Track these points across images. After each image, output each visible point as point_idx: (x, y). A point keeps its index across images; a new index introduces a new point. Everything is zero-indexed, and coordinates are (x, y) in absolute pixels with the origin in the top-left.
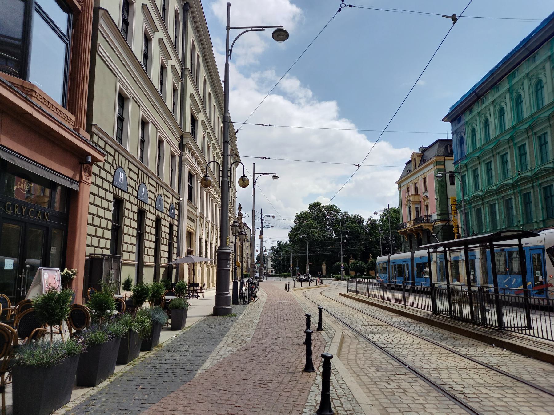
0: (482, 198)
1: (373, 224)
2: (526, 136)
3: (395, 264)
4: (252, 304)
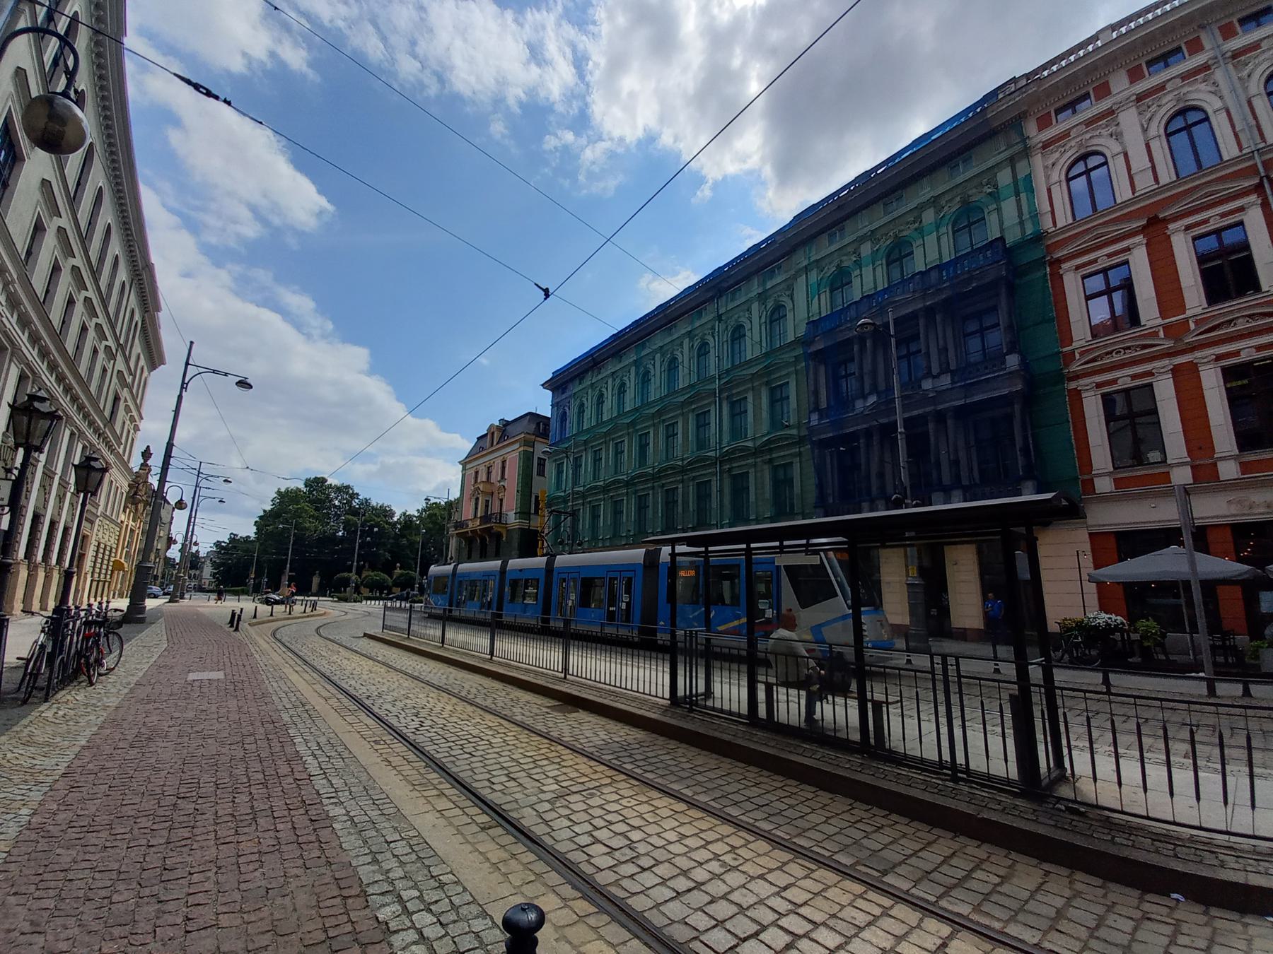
0: (583, 495)
1: (407, 521)
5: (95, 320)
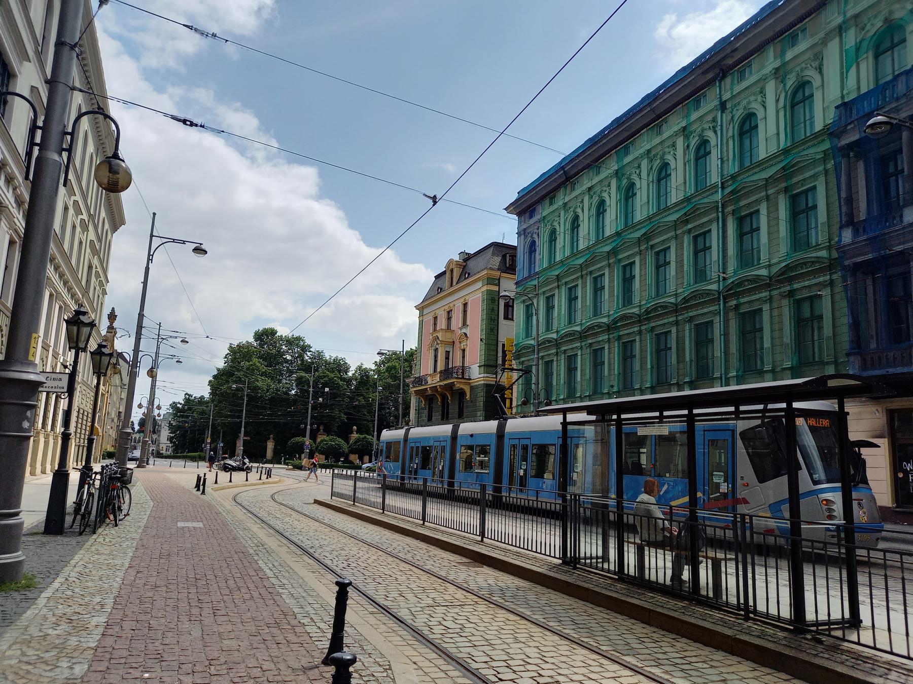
0: (557, 344)
1: (364, 376)
2: (673, 233)
3: (418, 445)
4: (106, 533)
5: (73, 198)
